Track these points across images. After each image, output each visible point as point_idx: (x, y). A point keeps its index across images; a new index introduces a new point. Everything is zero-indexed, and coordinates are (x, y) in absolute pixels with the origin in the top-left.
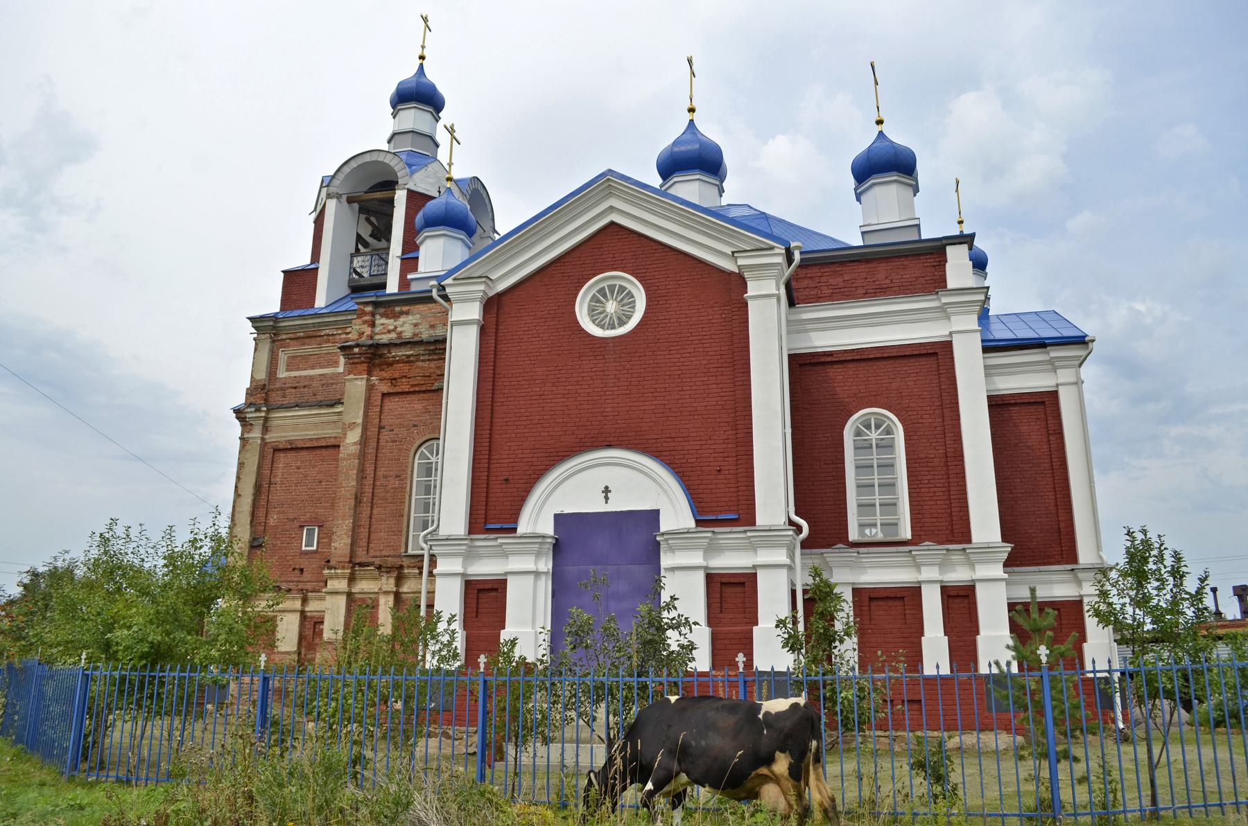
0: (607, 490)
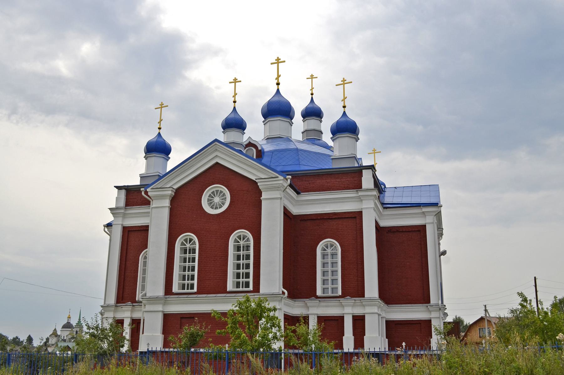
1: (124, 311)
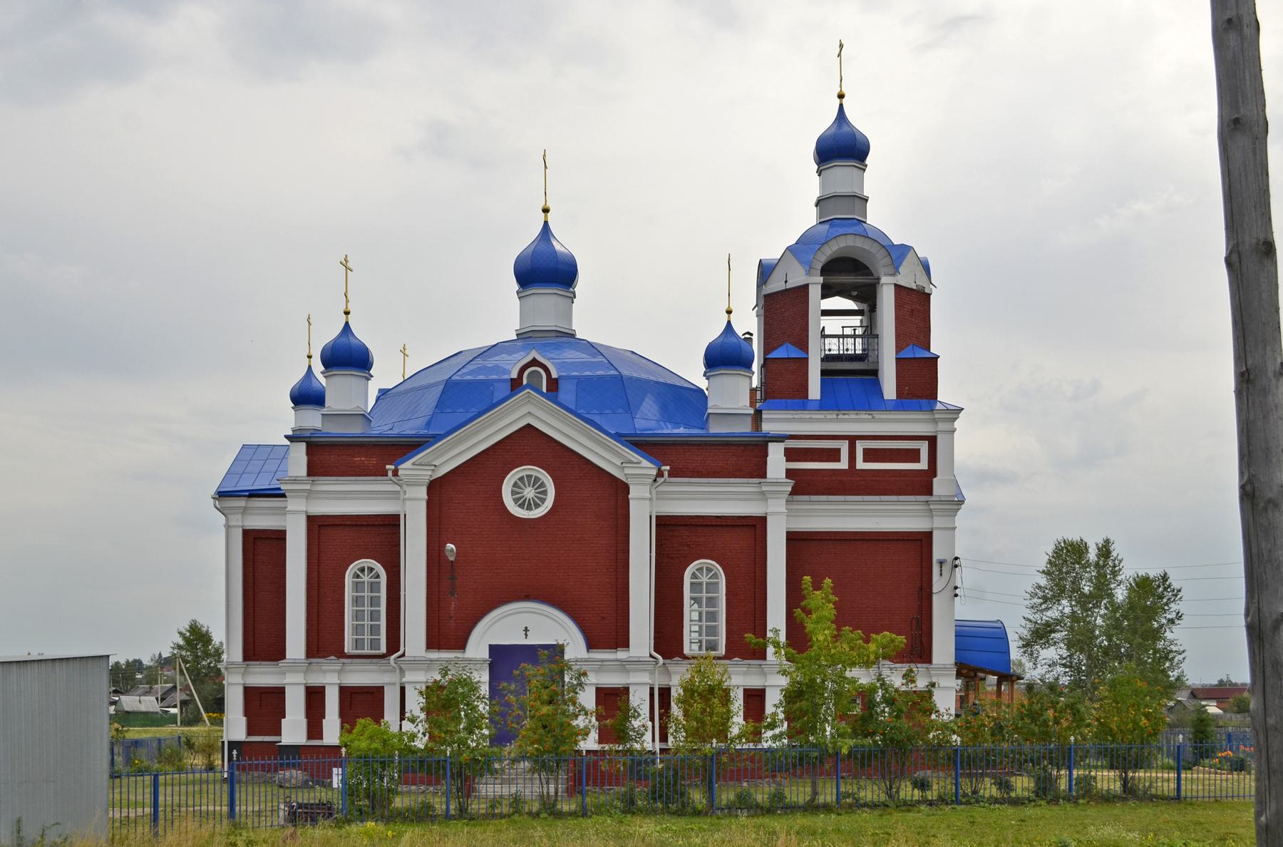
0: (526, 630)
1: (325, 672)
